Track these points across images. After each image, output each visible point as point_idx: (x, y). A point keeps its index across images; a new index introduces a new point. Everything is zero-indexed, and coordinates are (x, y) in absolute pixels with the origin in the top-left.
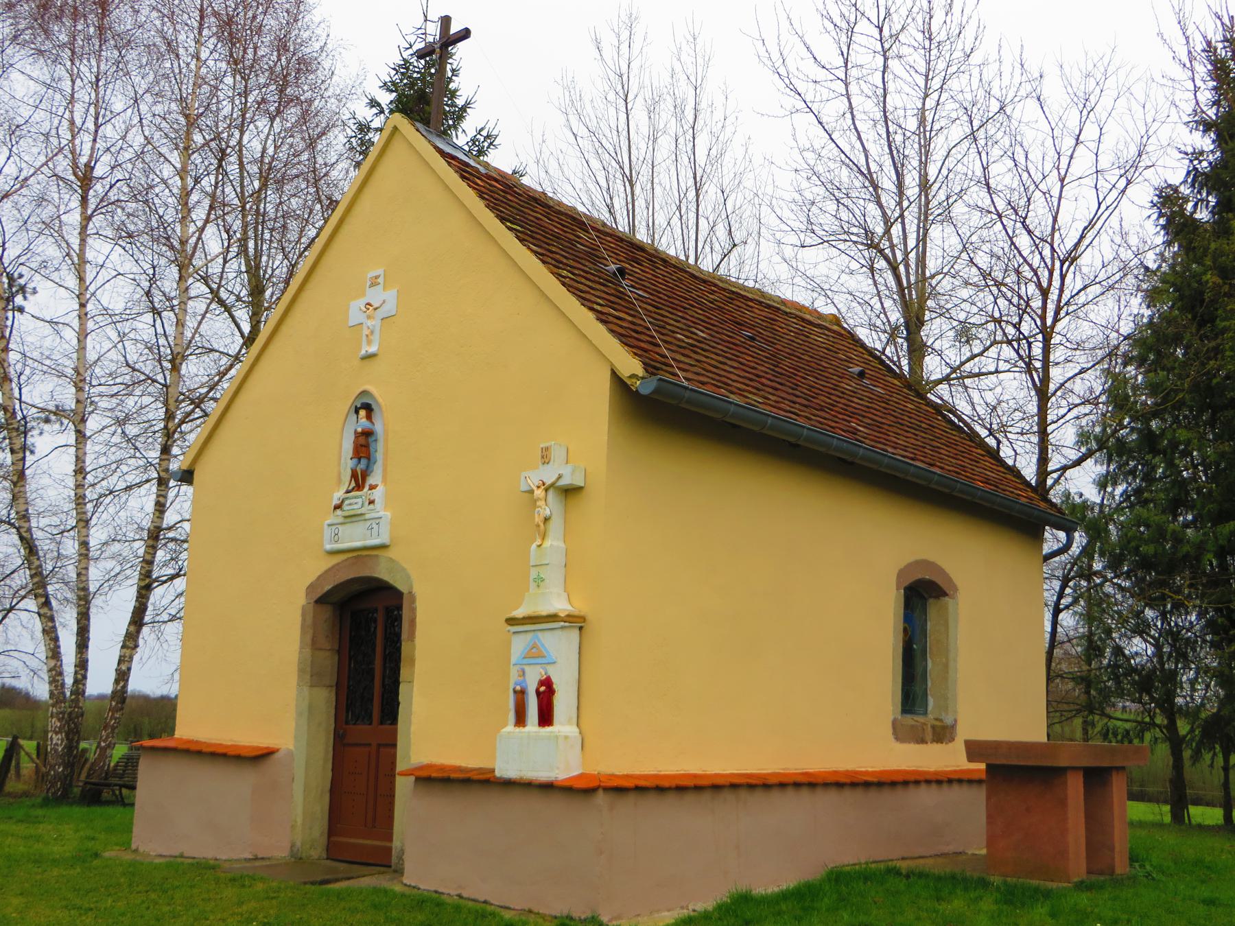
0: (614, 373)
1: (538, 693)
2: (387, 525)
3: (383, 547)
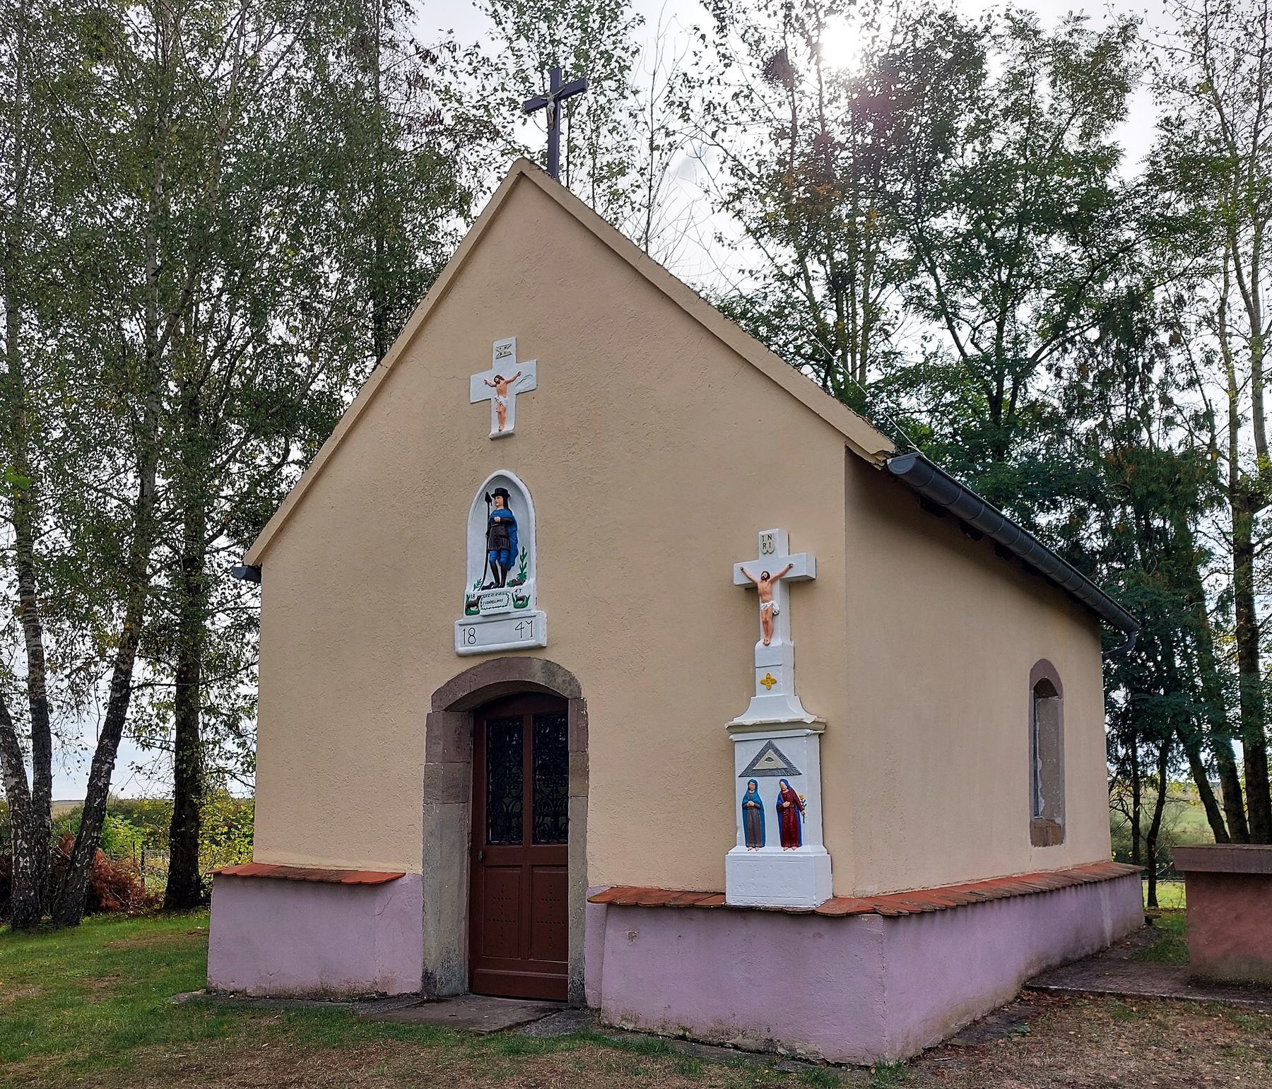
0: (848, 450)
1: (780, 809)
2: (527, 624)
3: (540, 648)
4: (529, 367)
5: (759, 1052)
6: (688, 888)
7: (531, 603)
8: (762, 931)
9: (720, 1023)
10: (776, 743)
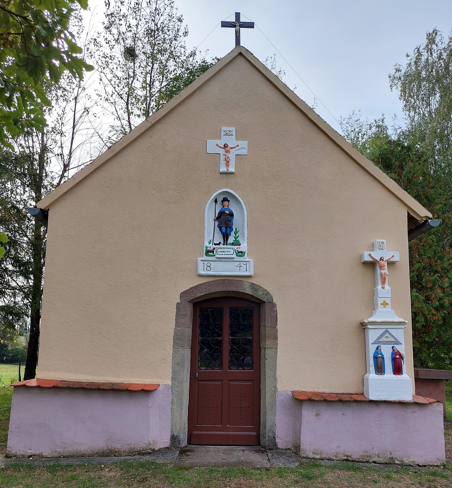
0: (409, 215)
3: (250, 277)
4: (244, 144)
5: (386, 463)
6: (333, 392)
7: (246, 254)
8: (386, 411)
9: (366, 452)
10: (389, 330)
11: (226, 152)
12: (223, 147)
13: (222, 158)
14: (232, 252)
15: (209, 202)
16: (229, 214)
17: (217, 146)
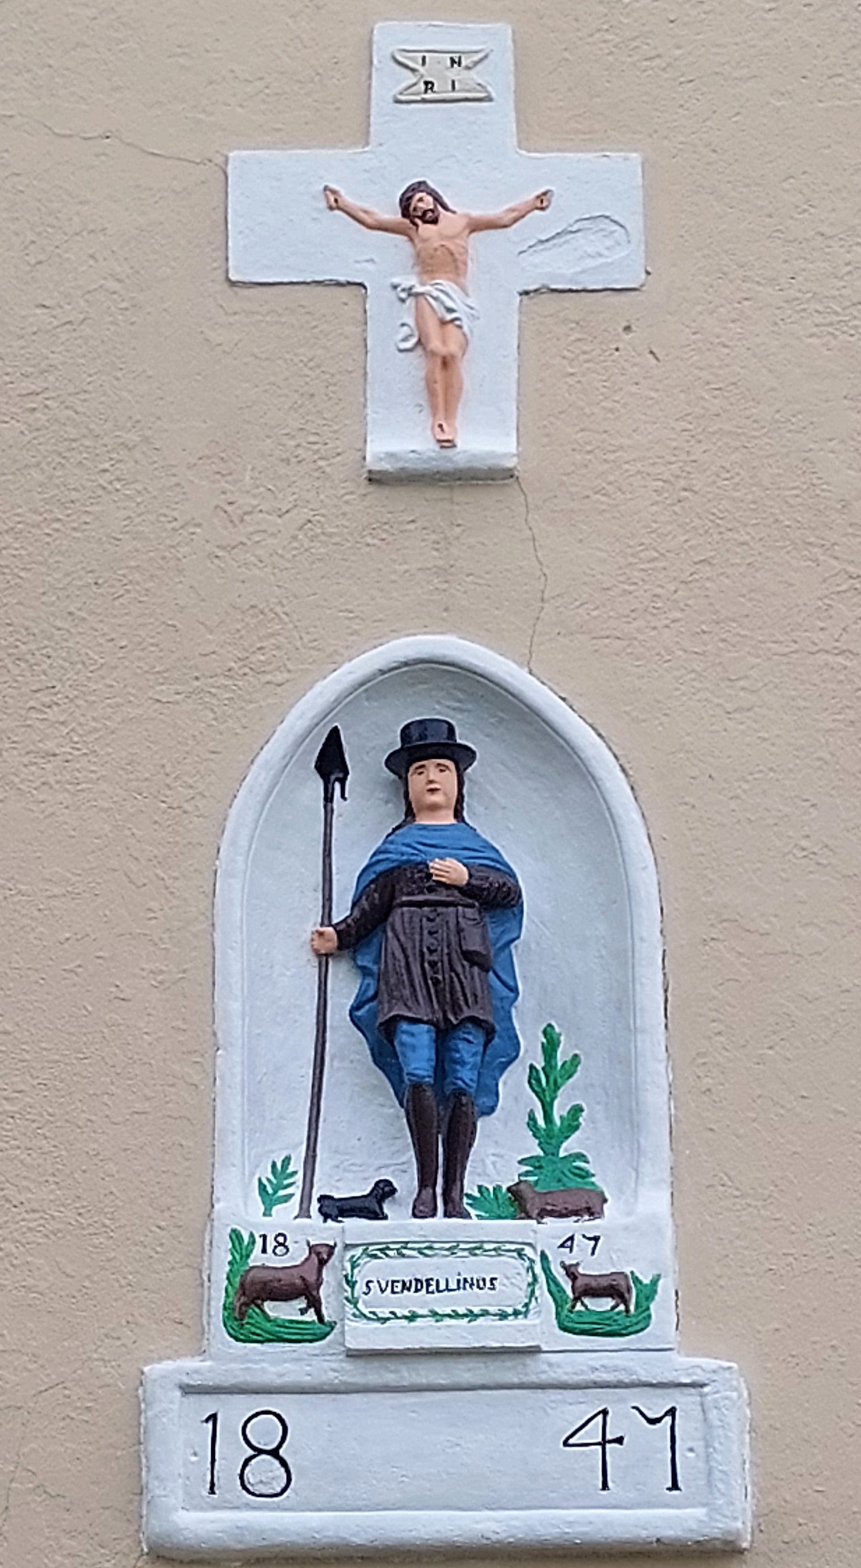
4: (604, 180)
7: (662, 1309)
11: (428, 264)
12: (392, 214)
13: (389, 325)
14: (511, 1291)
15: (258, 776)
16: (469, 891)
17: (336, 205)
